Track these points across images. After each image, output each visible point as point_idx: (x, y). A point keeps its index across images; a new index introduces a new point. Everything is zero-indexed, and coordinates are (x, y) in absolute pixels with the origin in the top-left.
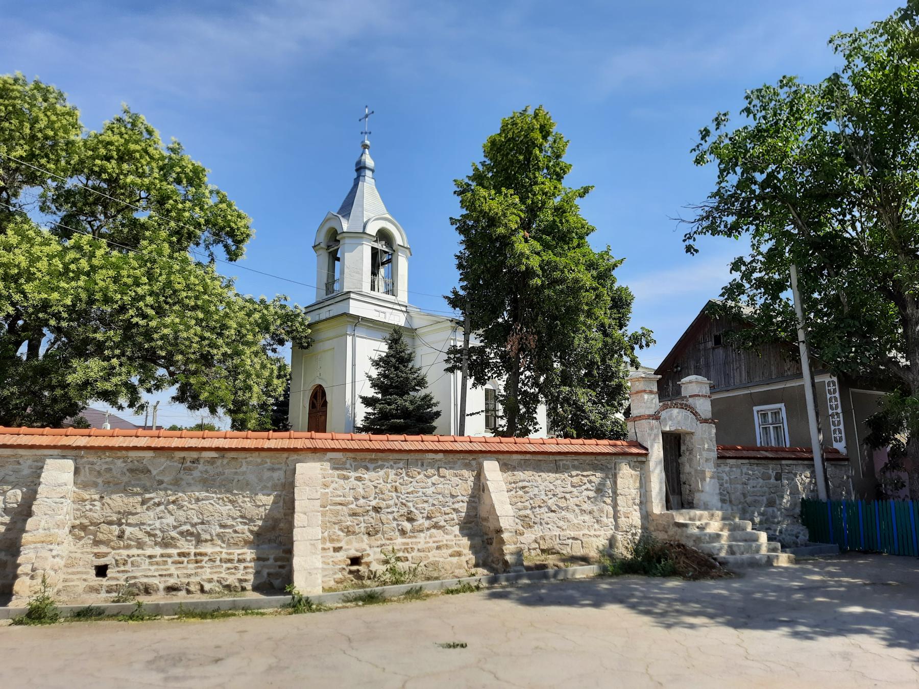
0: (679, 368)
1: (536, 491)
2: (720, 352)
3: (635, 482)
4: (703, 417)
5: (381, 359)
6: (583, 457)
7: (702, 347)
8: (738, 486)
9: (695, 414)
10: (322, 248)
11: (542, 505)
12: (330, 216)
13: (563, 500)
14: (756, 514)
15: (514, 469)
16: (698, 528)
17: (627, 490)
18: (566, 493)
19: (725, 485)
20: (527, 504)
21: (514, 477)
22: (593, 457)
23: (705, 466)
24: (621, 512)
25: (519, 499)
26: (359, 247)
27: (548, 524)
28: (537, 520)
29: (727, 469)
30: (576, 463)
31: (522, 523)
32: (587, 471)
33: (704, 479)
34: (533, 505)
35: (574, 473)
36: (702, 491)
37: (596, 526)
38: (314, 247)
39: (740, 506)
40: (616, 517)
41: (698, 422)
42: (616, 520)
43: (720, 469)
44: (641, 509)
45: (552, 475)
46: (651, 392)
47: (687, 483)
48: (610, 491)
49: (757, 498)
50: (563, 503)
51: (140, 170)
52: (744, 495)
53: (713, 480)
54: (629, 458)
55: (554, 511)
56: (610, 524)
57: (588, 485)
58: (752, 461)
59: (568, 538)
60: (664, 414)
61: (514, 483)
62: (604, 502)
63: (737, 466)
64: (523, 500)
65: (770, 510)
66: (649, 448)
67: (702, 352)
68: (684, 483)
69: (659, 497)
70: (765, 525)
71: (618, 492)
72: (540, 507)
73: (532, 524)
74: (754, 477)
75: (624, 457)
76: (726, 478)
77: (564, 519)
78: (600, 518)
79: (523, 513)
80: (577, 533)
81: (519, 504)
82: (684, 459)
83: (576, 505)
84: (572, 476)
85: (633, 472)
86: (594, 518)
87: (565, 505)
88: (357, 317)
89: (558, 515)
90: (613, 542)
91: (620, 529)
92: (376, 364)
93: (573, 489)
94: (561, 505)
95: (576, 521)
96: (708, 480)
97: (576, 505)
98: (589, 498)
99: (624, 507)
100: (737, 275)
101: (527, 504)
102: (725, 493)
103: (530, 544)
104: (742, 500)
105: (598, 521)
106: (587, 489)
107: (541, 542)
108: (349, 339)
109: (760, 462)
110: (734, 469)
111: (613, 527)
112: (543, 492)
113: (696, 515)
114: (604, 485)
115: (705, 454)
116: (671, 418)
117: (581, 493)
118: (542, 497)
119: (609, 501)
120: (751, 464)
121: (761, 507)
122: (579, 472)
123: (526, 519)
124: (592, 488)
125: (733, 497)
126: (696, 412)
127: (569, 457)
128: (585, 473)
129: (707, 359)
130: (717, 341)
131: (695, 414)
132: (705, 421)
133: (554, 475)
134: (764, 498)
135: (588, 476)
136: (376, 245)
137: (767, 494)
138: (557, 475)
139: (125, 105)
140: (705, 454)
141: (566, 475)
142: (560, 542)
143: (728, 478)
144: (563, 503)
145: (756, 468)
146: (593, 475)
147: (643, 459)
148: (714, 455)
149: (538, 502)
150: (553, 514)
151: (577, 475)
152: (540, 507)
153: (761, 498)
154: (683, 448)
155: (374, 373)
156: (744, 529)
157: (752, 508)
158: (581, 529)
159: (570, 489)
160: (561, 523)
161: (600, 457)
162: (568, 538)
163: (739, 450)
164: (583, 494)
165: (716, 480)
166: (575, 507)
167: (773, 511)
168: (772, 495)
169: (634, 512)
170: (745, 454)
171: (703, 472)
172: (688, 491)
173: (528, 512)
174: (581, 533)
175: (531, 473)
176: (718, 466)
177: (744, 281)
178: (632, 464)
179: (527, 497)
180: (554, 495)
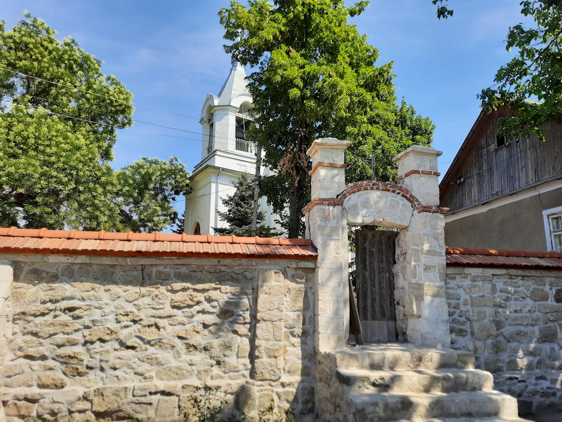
0: (462, 179)
1: (97, 315)
2: (504, 153)
3: (295, 300)
4: (424, 203)
5: (231, 199)
6: (195, 262)
7: (484, 151)
8: (487, 309)
9: (411, 199)
10: (205, 122)
11: (107, 338)
12: (208, 96)
13: (153, 329)
14: (521, 353)
15: (54, 278)
16: (374, 385)
17: (275, 312)
18: (160, 317)
19: (463, 308)
20: (78, 337)
21: (51, 293)
22: (214, 261)
23: (423, 278)
24: (262, 349)
25: (58, 329)
26: (226, 117)
27: (115, 369)
28: (94, 363)
29: (467, 282)
30: (184, 270)
31: (63, 367)
32: (203, 282)
33: (420, 298)
34: (88, 338)
35: (178, 286)
36: (419, 317)
37: (216, 370)
38: (200, 122)
39: (489, 341)
40: (252, 357)
41: (416, 212)
42: (252, 362)
43: (452, 283)
44: (303, 343)
45: (133, 290)
46: (332, 166)
47: (401, 302)
48: (247, 315)
49: (522, 328)
50: (151, 334)
51: (34, 57)
52: (498, 324)
53: (438, 300)
54: (283, 263)
55: (133, 348)
56: (241, 367)
57: (206, 306)
58: (513, 272)
59: (151, 393)
60: (352, 200)
61: (51, 301)
62: (235, 332)
63: (484, 279)
64: (67, 330)
65: (547, 347)
66: (319, 247)
67: (485, 157)
68: (398, 304)
69: (332, 326)
70: (537, 371)
71: (259, 316)
72: (102, 340)
73: (82, 369)
74: (516, 296)
75: (273, 261)
76: (464, 296)
77: (150, 360)
78: (222, 359)
79: (68, 350)
80: (172, 383)
81: (61, 336)
82: (397, 268)
83: (180, 338)
84: (173, 291)
85: (292, 285)
86: (211, 357)
87: (155, 337)
88: (218, 168)
89: (140, 354)
90: (242, 398)
91: (258, 376)
92: (226, 202)
93: (175, 311)
94: (147, 337)
95: (174, 363)
96: (428, 299)
97: (180, 338)
98: (205, 326)
99: (267, 340)
100: (515, 52)
101: (78, 337)
102: (463, 319)
103: (71, 403)
104: (494, 332)
105: (218, 363)
106: (203, 312)
107: (96, 400)
108: (213, 186)
109: (527, 273)
110: (480, 283)
111: (247, 373)
112: (112, 317)
113: (383, 359)
114: (237, 305)
115: (424, 259)
116: (366, 204)
117: (192, 316)
118: (109, 325)
119: (243, 329)
120: (511, 277)
121: (530, 342)
122: (188, 285)
123: (71, 361)
124: (212, 310)
125: (476, 325)
126: (412, 196)
127: (166, 261)
128: (200, 286)
129: (489, 163)
130: (500, 142)
131: (411, 199)
132: (426, 209)
133: (137, 289)
134: (536, 329)
135: (203, 291)
136: (241, 116)
137: (541, 322)
138: (144, 290)
139: (26, 12)
140: (424, 259)
141: (163, 289)
142: (135, 399)
143: (468, 297)
144: (151, 334)
145: (521, 282)
146: (215, 289)
147: (310, 265)
148: (442, 260)
149: (98, 332)
150: (131, 352)
151: (184, 290)
152: (102, 340)
153: (530, 328)
154: (398, 251)
155: (224, 209)
156: (476, 388)
157: (514, 345)
158: (184, 377)
159: (168, 310)
160: (143, 367)
161: (228, 261)
162: (151, 393)
163: (491, 255)
164: (195, 319)
165: (444, 300)
166: (178, 342)
167: (553, 349)
168: (550, 324)
169: (290, 349)
170: (501, 260)
171: (420, 287)
172: (402, 315)
173: (79, 349)
174: (180, 384)
175: (88, 285)
176: (447, 278)
177: (525, 58)
178: (290, 272)
179: (77, 324)
180: (135, 322)
